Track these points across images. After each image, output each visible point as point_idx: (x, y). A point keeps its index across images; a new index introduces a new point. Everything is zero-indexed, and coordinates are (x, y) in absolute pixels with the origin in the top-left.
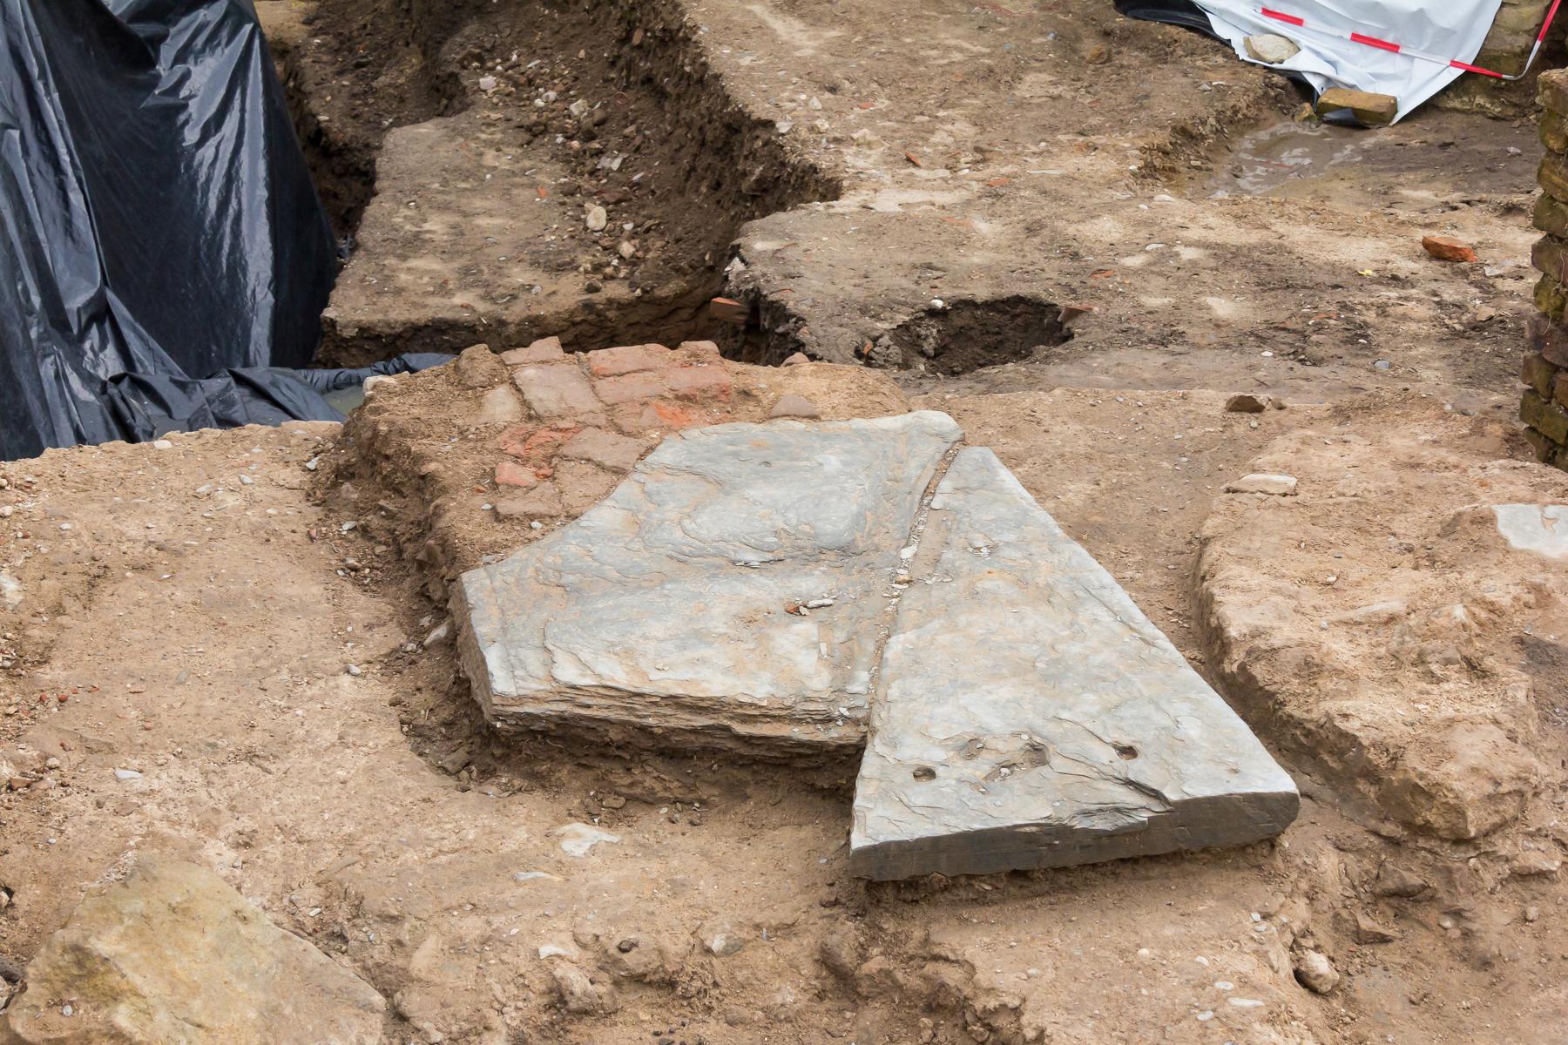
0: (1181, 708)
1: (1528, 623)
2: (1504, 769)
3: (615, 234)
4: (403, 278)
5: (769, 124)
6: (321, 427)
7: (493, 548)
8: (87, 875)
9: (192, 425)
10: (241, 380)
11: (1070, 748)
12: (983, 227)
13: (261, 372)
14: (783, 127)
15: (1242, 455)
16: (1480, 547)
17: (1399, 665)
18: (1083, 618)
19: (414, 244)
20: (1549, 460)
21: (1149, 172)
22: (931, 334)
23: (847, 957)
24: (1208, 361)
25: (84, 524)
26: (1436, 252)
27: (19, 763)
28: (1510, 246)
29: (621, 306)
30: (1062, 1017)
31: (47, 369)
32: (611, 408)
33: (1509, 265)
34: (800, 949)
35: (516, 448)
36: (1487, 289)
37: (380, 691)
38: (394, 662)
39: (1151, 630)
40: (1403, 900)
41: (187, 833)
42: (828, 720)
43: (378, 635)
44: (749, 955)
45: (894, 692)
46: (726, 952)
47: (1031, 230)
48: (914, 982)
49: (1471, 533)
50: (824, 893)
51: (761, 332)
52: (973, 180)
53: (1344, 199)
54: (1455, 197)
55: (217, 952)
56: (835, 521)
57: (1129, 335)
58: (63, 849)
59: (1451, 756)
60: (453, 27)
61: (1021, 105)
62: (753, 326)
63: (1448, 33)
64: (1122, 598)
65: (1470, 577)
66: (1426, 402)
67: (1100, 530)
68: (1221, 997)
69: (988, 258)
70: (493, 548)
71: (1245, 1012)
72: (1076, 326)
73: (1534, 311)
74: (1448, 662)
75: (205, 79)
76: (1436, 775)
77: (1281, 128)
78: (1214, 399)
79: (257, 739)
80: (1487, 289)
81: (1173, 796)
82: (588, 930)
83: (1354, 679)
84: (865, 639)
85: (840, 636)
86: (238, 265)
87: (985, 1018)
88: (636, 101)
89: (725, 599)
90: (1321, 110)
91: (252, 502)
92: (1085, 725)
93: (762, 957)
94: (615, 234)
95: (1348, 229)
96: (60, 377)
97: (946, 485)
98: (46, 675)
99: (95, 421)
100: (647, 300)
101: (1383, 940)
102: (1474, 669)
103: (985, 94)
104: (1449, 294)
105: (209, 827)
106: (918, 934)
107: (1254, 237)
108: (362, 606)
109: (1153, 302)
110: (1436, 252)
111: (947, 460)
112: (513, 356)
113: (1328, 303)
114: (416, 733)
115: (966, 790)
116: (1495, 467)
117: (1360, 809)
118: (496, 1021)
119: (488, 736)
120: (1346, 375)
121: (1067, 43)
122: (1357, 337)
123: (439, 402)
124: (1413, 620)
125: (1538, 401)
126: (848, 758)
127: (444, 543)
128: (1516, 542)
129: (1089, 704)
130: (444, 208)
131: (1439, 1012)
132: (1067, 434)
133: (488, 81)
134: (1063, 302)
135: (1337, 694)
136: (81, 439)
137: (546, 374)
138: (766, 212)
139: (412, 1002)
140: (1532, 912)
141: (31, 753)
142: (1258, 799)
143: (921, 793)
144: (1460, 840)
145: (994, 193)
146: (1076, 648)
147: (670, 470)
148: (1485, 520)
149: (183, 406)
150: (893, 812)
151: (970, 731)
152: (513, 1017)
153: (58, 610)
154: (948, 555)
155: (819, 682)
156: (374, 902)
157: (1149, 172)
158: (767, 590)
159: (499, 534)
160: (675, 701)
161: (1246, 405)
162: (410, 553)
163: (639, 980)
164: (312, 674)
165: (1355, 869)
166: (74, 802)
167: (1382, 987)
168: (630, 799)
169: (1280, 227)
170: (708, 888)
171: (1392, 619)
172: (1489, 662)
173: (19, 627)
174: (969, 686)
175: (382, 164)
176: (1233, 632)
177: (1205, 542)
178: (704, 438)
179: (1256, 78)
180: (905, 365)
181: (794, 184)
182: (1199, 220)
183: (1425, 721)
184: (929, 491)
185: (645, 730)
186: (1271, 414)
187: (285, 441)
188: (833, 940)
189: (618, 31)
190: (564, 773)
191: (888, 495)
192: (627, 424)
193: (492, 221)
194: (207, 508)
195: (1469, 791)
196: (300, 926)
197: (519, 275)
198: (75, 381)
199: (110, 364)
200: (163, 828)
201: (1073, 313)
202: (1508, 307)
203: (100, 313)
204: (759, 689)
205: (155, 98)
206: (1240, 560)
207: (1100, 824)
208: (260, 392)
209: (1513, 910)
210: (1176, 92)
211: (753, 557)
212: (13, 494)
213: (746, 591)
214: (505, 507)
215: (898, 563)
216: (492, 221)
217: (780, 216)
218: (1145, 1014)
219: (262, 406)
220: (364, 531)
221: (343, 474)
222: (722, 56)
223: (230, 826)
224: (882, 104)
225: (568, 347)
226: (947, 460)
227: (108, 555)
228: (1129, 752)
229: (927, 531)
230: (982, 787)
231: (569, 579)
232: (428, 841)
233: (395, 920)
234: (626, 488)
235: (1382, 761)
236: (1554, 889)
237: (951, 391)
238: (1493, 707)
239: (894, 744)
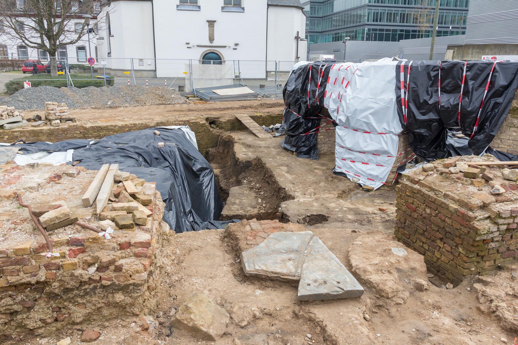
0: (346, 276)
1: (397, 265)
2: (394, 288)
3: (262, 203)
4: (232, 208)
5: (285, 189)
6: (221, 230)
7: (246, 249)
8: (187, 294)
9: (203, 229)
10: (210, 222)
11: (330, 282)
12: (315, 204)
13: (212, 221)
14: (287, 189)
15: (354, 239)
16: (390, 254)
17: (378, 271)
18: (331, 262)
19: (234, 203)
20: (398, 241)
21: (339, 197)
22: (308, 219)
23: (297, 312)
24: (348, 225)
25: (189, 243)
26: (381, 210)
27: (178, 277)
28: (392, 210)
29: (263, 213)
30: (329, 323)
31: (183, 220)
32: (263, 229)
33: (391, 212)
34: (290, 310)
35: (250, 234)
36: (388, 215)
37: (230, 269)
38: (232, 265)
39: (342, 264)
40: (379, 307)
41: (202, 289)
42: (294, 276)
43: (229, 261)
44: (282, 311)
45: (304, 272)
46: (279, 310)
47: (322, 205)
48: (307, 316)
49: (388, 252)
50: (294, 302)
51: (284, 218)
52: (313, 197)
53: (367, 202)
54: (383, 202)
55: (206, 307)
56: (295, 246)
57: (336, 220)
58: (184, 290)
59: (386, 285)
60: (241, 174)
61: (320, 187)
62: (282, 217)
63: (381, 179)
64: (337, 259)
65: (388, 258)
66: (381, 232)
67: (333, 249)
68: (353, 321)
69: (316, 209)
70: (246, 249)
71: (356, 323)
72: (329, 219)
73: (396, 219)
74: (385, 271)
75: (206, 180)
76: (384, 288)
77: (357, 191)
78: (349, 230)
79: (212, 275)
80: (388, 215)
81: (345, 290)
82: (259, 306)
83: (371, 273)
84: (300, 264)
85: (296, 264)
86: (209, 206)
87: (317, 322)
88: (266, 185)
89: (280, 258)
90: (363, 189)
91: (212, 240)
92: (332, 278)
93: (284, 311)
94: (262, 203)
95: (368, 206)
96: (185, 221)
97: (311, 242)
98: (183, 264)
99: (189, 227)
100: (267, 213)
101: (377, 313)
102: (389, 272)
103: (315, 185)
104: (383, 216)
105: (205, 288)
106: (308, 309)
107: (354, 207)
108: (228, 256)
109: (340, 216)
110: (381, 210)
111: (311, 238)
112: (250, 221)
113: (365, 216)
114: (235, 275)
115: (315, 288)
116: (391, 242)
117: (373, 293)
118: (245, 319)
119: (245, 276)
120: (368, 227)
121: (327, 178)
122: (369, 222)
123: (239, 227)
124: (380, 264)
125: (397, 232)
126: (297, 282)
127: (239, 248)
128: (395, 253)
129: (333, 275)
130: (238, 199)
131: (385, 325)
132: (328, 235)
133: (245, 181)
134: (327, 215)
135: (369, 275)
136: (187, 230)
137: (254, 224)
138: (284, 201)
139: (233, 316)
140: (399, 309)
141: (180, 276)
142: (358, 291)
143: (308, 288)
144: (388, 298)
145: (317, 199)
146: (331, 267)
147: (272, 238)
148: (390, 250)
149: (202, 226)
150: (304, 290)
151: (315, 278)
152: (248, 319)
153: (185, 255)
154: (312, 252)
155: (293, 270)
156: (228, 301)
157: (339, 197)
158: (285, 256)
159: (247, 246)
160: (272, 272)
161: (354, 232)
162: (235, 251)
163: (266, 314)
164: (220, 266)
165: (372, 302)
166: (186, 283)
167: (376, 320)
168: (265, 286)
169: (358, 205)
170: (277, 301)
171: (377, 264)
172: (391, 271)
173: (179, 257)
174: (315, 272)
175: (230, 192)
176: (353, 265)
177: (349, 252)
178: (276, 234)
179: (354, 184)
180: (304, 224)
181: (288, 197)
182: (346, 204)
183: (382, 280)
184: (309, 243)
185: (268, 276)
186: (358, 233)
187: (217, 232)
188: (295, 309)
189: (263, 175)
190: (256, 282)
191: (303, 243)
192: (266, 231)
193: (245, 201)
194: (206, 241)
195: (389, 291)
196: (217, 303)
197: (249, 209)
198: (187, 221)
199: (191, 219)
200: (198, 288)
201: (328, 217)
202: (391, 218)
203: (190, 212)
204: (285, 271)
205: (199, 182)
206: (354, 254)
207: (335, 293)
208: (212, 224)
209: (396, 309)
210: (342, 186)
211: (284, 251)
212: (179, 238)
213: (283, 256)
214: (248, 243)
215: (305, 253)
216: (245, 201)
217: (286, 202)
218: (341, 323)
219: (212, 226)
220: (228, 245)
221: (225, 237)
222: (278, 179)
223: (208, 288)
224: (301, 186)
225: (257, 220)
226: (311, 238)
227: (192, 247)
228: (339, 283)
229: (309, 249)
230: (317, 287)
231: (257, 254)
232: (236, 292)
233: (231, 303)
234: (265, 241)
235: (376, 285)
236: (402, 306)
237: (311, 227)
238: (392, 278)
239: (304, 280)
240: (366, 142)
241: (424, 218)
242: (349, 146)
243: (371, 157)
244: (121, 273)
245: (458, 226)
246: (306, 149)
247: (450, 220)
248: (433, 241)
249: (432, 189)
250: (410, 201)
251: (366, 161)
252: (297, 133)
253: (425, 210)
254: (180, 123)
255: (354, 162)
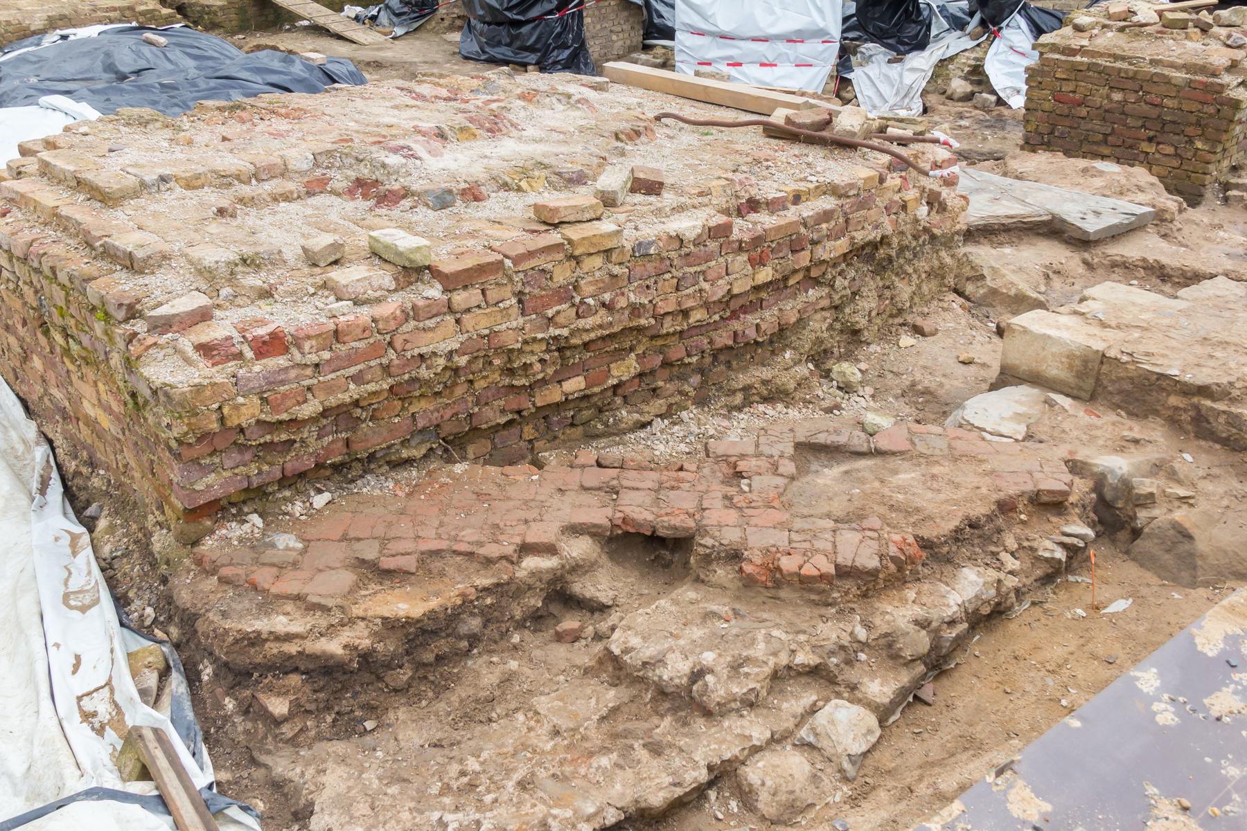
160: (1007, 217)
240: (772, 13)
241: (1106, 111)
242: (725, 27)
243: (782, 47)
244: (947, 214)
245: (1194, 107)
246: (567, 52)
247: (1176, 101)
248: (1131, 147)
249: (1116, 57)
250: (1067, 87)
251: (771, 59)
252: (535, 12)
253: (1108, 97)
254: (112, 14)
255: (740, 65)
